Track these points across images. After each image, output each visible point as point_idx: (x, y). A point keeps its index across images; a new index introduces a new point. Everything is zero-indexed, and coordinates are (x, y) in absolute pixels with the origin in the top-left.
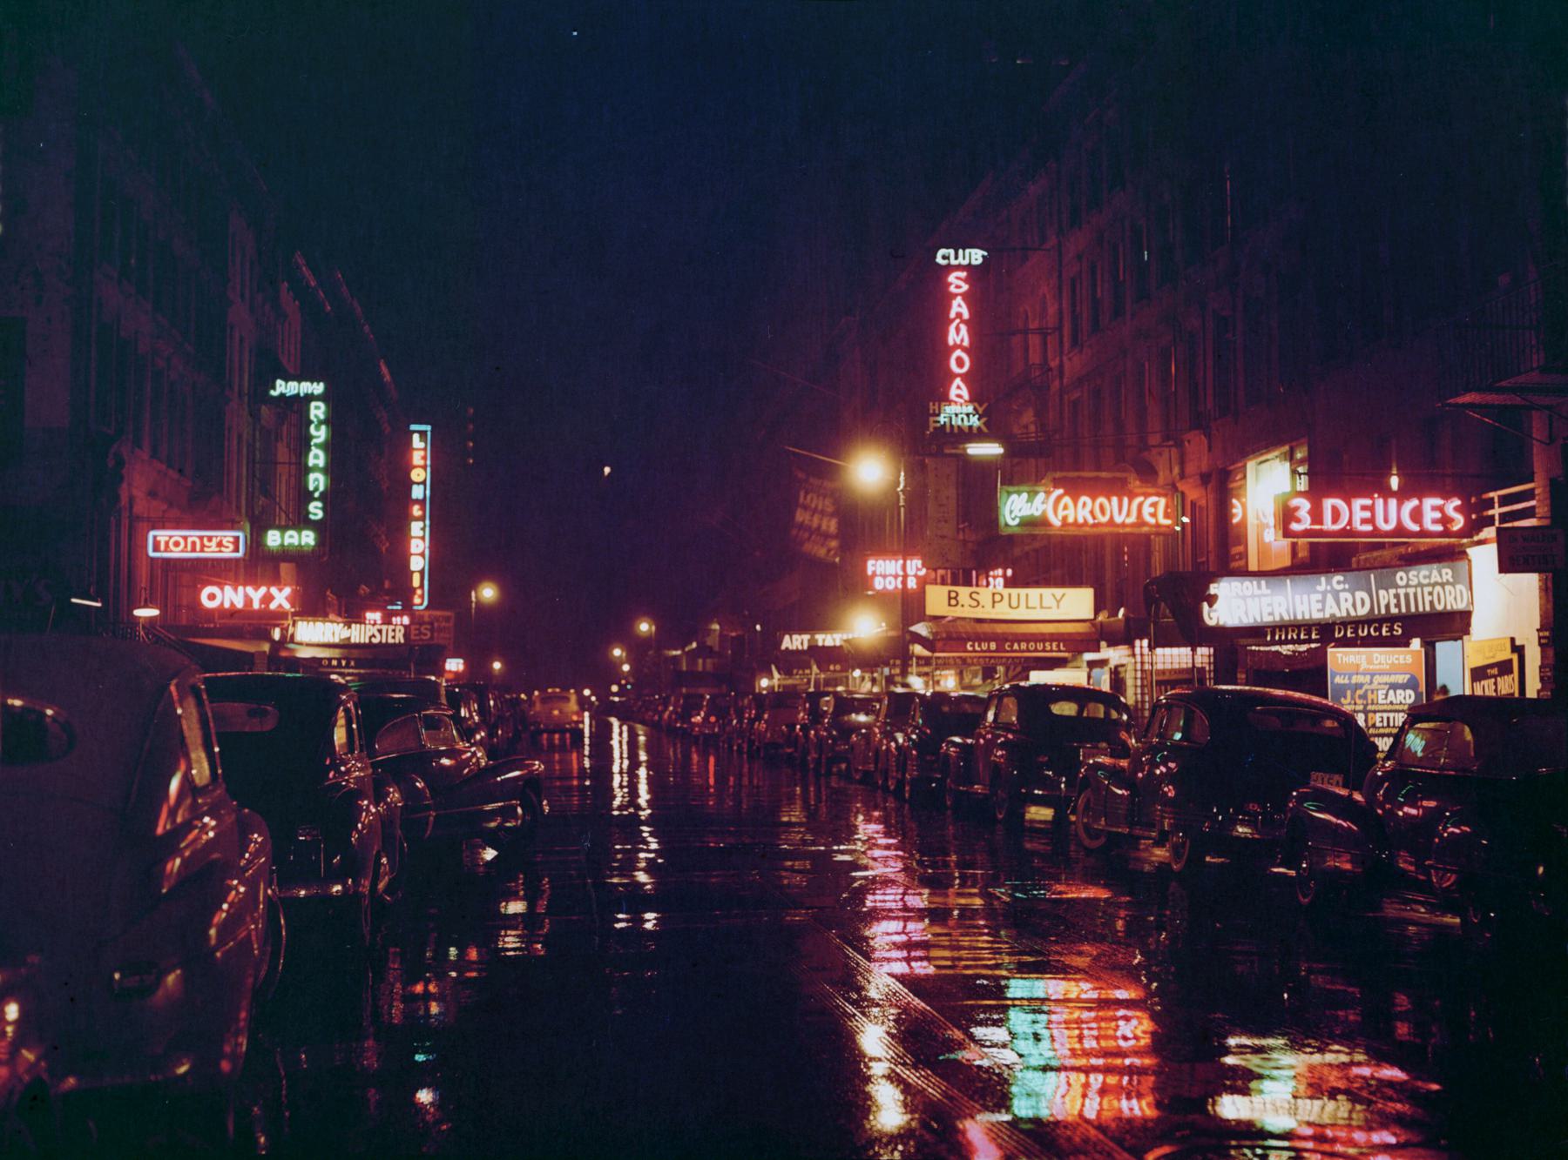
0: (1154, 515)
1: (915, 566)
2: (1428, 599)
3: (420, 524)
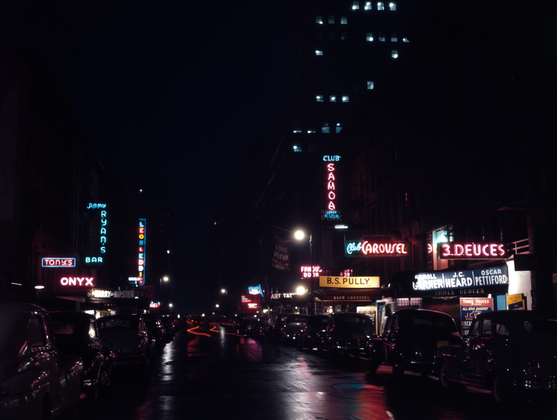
0: (400, 250)
1: (317, 269)
2: (493, 280)
3: (142, 254)
